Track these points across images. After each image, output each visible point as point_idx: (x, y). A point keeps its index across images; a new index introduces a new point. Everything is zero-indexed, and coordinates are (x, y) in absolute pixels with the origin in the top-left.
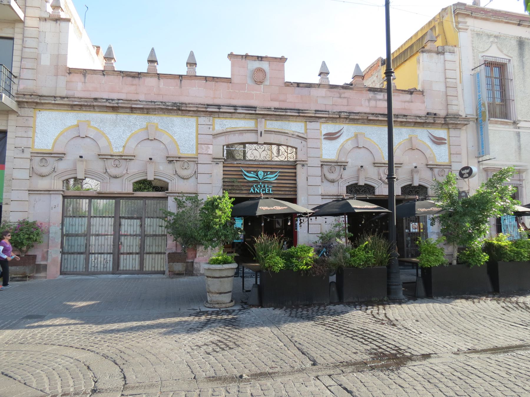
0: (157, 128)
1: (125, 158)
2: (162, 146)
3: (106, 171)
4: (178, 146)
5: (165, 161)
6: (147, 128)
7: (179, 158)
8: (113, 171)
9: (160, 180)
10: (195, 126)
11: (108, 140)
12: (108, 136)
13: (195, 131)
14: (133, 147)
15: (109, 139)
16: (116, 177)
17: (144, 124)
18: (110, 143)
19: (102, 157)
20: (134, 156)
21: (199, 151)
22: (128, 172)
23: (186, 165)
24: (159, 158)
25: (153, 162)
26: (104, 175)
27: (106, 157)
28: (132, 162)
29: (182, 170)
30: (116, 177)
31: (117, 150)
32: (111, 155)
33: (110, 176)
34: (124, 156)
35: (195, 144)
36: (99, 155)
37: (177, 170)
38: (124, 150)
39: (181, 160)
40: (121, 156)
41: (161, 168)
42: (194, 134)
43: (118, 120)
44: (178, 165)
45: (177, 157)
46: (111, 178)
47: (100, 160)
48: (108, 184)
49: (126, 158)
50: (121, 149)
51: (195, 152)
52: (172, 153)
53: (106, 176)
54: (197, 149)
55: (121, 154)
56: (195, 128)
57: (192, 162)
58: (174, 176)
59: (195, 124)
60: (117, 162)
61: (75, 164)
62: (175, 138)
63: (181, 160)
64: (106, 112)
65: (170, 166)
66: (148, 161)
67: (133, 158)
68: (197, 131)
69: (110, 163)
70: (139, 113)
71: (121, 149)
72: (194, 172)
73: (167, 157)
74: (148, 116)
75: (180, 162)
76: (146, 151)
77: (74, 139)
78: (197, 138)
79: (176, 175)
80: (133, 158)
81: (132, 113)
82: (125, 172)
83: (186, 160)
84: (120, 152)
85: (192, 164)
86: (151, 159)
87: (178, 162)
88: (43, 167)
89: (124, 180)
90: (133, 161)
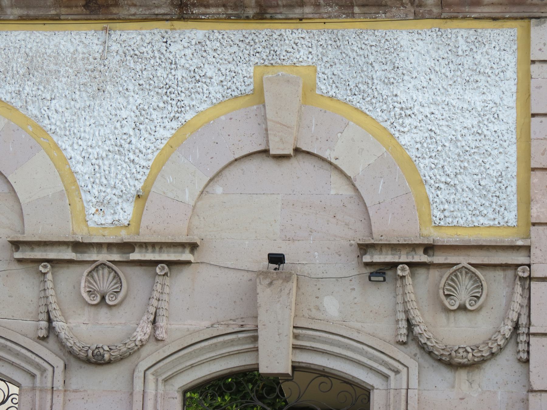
0: (309, 90)
1: (150, 257)
2: (338, 188)
3: (51, 328)
4: (423, 183)
5: (349, 267)
6: (258, 95)
7: (429, 248)
8: (85, 328)
9: (324, 374)
10: (511, 73)
11: (61, 162)
12: (64, 144)
13: (510, 100)
14: (188, 197)
15: (66, 160)
16: (96, 360)
17: (246, 74)
18: (70, 179)
19: (381, 264)
20: (193, 247)
21: (537, 212)
22: (160, 333)
23: (463, 293)
24: (322, 250)
25: (287, 279)
26: (38, 348)
27: (52, 255)
28: (182, 279)
29: (442, 318)
30: (96, 360)
31: (107, 215)
32: (77, 246)
33: (71, 352)
34: (144, 245)
35: (513, 170)
36: (16, 245)
37: (417, 317)
38: (139, 214)
39: (439, 259)
40: (127, 246)
41: (332, 306)
42: (510, 116)
43: (113, 61)
44: (419, 289)
45: (413, 247)
46: (74, 363)
47: (17, 266)
48: (59, 400)
49: (38, 254)
50: (126, 212)
51: (511, 217)
52: (392, 224)
53: (47, 353)
54: (526, 200)
55: (125, 236)
56: (511, 86)
57: (499, 274)
58: (400, 354)
59: (510, 60)
60: (104, 281)
61: (251, 298)
62: (404, 140)
63: (439, 259)
64: (56, 18)
65: (381, 297)
66: (263, 274)
67: (186, 256)
68: (525, 94)
69: (69, 284)
70: (217, 19)
71: (126, 212)
72: (507, 329)
73: (364, 248)
74: (263, 31)
75: (434, 273)
76: (248, 218)
77: (236, 171)
78: (525, 138)
79: (413, 348)
80: (186, 256)
81: (181, 18)
82: (143, 331)
83: (463, 260)
84: (116, 225)
85: (497, 285)
86: (276, 259)
87: (422, 273)
88: (462, 317)
89: (139, 374)
90: (187, 272)
